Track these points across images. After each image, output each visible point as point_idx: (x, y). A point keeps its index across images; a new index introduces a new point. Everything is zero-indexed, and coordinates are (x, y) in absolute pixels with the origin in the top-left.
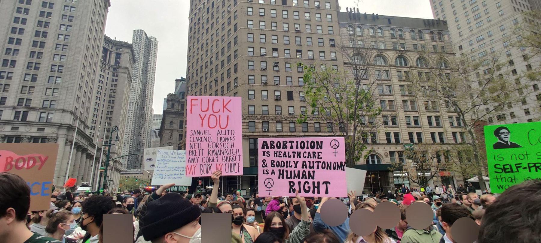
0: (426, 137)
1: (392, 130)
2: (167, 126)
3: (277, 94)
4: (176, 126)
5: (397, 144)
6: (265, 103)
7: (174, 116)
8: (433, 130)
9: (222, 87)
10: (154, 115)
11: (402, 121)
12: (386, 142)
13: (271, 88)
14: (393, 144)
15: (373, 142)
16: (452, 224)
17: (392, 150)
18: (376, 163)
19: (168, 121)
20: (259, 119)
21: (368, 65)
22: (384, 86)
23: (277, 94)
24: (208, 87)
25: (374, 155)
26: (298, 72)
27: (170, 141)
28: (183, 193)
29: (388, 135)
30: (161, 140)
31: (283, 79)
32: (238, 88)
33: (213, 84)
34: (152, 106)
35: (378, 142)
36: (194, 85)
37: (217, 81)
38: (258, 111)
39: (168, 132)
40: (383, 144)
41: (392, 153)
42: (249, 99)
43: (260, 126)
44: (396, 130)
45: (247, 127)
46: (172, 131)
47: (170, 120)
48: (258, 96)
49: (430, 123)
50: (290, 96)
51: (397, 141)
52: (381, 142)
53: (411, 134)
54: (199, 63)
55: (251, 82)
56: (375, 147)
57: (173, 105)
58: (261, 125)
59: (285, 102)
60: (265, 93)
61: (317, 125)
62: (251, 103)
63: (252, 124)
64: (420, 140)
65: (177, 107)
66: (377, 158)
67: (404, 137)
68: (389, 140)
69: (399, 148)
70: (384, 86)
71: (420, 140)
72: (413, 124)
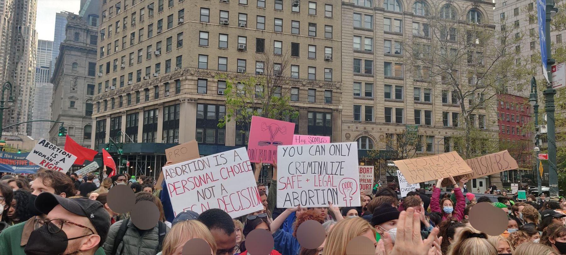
0: (437, 118)
1: (394, 105)
2: (67, 68)
3: (242, 41)
4: (83, 70)
5: (398, 125)
6: (223, 53)
7: (79, 54)
8: (446, 108)
9: (160, 21)
10: (39, 41)
11: (409, 94)
12: (384, 121)
13: (233, 31)
14: (393, 125)
15: (366, 120)
16: (340, 210)
17: (390, 132)
18: (367, 148)
19: (68, 60)
20: (213, 77)
21: (376, 9)
22: (393, 43)
23: (242, 41)
24: (137, 17)
25: (366, 137)
26: (275, 10)
27: (72, 95)
28: (449, 214)
29: (388, 111)
30: (55, 89)
31: (252, 18)
32: (185, 27)
33: (145, 12)
34: (34, 26)
35: (373, 121)
36: (114, 9)
37: (152, 10)
38: (213, 65)
39: (70, 79)
40: (379, 124)
41: (389, 136)
42: (200, 46)
43: (213, 87)
44: (399, 105)
45: (196, 87)
46: (76, 78)
47: (73, 60)
48: (213, 42)
49: (444, 100)
50: (260, 45)
51: (399, 120)
52: (378, 121)
53: (417, 113)
54: (128, 8)
55: (205, 19)
56: (369, 127)
57: (77, 34)
58: (215, 85)
59: (251, 54)
60: (223, 38)
61: (295, 92)
62: (203, 51)
63: (202, 83)
64: (428, 122)
65: (84, 39)
66: (369, 141)
67: (409, 116)
68: (388, 119)
69: (400, 129)
70: (393, 43)
71: (428, 122)
72: (422, 99)
